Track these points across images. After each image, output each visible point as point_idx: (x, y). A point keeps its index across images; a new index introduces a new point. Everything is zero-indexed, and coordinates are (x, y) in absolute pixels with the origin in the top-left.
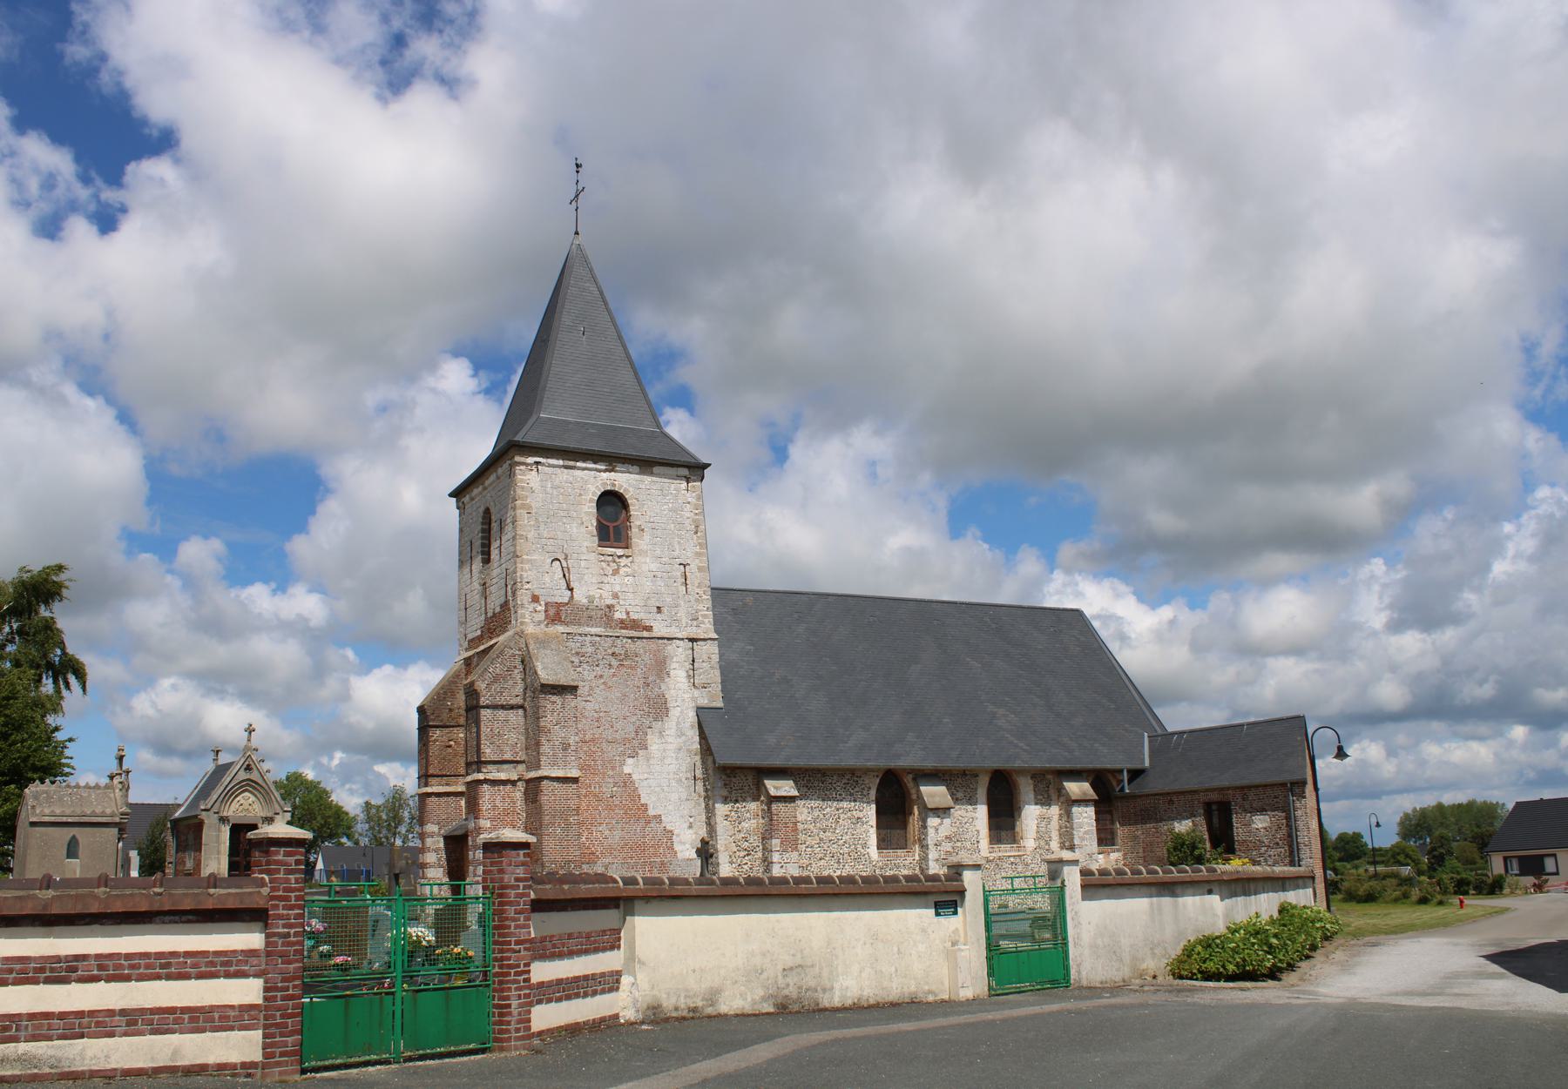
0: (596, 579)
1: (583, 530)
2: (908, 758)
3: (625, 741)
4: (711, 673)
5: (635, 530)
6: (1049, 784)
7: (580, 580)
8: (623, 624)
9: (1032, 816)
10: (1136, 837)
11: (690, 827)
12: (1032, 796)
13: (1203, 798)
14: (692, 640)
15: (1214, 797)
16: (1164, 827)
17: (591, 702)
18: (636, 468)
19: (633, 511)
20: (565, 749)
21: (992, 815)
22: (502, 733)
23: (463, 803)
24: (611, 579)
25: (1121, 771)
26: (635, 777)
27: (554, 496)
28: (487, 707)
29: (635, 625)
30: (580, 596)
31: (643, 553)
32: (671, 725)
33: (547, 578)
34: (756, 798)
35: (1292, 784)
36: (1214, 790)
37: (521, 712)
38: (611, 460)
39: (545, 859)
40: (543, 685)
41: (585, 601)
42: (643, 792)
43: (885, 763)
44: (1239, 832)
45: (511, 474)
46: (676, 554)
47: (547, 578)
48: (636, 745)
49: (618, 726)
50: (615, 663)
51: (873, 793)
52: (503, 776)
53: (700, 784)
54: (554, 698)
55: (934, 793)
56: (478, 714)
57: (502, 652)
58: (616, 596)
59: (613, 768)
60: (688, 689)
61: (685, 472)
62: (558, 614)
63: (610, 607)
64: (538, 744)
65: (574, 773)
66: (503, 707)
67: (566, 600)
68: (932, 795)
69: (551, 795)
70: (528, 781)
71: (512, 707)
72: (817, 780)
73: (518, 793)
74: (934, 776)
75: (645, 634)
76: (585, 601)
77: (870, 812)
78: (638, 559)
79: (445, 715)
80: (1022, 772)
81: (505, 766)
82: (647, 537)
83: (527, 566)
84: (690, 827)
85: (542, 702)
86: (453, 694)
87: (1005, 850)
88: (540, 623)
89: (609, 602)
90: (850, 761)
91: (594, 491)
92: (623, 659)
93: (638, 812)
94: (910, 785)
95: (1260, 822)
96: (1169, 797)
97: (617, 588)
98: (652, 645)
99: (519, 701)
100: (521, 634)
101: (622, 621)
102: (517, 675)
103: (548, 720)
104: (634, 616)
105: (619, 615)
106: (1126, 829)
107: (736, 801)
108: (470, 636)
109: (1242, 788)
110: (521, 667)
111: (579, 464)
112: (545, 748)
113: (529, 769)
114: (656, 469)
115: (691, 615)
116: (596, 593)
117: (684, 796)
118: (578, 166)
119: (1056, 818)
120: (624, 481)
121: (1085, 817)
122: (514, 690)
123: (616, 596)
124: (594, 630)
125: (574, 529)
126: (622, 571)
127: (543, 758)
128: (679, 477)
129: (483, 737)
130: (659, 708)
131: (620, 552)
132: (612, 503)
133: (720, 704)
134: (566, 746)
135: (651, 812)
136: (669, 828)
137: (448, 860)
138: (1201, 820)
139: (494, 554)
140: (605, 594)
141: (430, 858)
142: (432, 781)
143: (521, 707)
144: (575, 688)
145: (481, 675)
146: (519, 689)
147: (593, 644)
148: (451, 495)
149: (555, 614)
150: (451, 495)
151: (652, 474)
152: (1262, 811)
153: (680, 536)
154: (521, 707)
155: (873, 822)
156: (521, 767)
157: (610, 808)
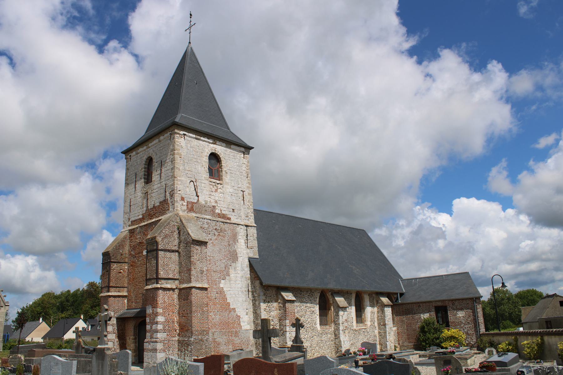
0: (208, 194)
1: (203, 169)
2: (332, 285)
3: (221, 271)
4: (254, 243)
5: (224, 172)
6: (375, 297)
7: (202, 192)
8: (219, 216)
9: (370, 312)
10: (403, 321)
11: (247, 314)
12: (369, 303)
13: (434, 304)
14: (247, 226)
15: (440, 304)
16: (416, 316)
17: (210, 250)
18: (224, 144)
19: (224, 163)
20: (202, 273)
21: (357, 311)
22: (169, 264)
23: (126, 301)
24: (214, 194)
25: (397, 294)
26: (225, 289)
27: (190, 151)
28: (162, 250)
29: (224, 216)
30: (202, 200)
31: (227, 183)
32: (239, 265)
33: (188, 190)
34: (276, 301)
35: (476, 298)
36: (439, 301)
37: (177, 254)
38: (215, 139)
39: (193, 329)
40: (193, 240)
41: (203, 203)
42: (228, 297)
43: (321, 287)
44: (451, 318)
45: (171, 138)
46: (240, 186)
47: (188, 190)
48: (225, 274)
49: (218, 264)
50: (217, 234)
51: (318, 300)
52: (169, 286)
53: (250, 294)
54: (197, 247)
55: (340, 300)
56: (157, 254)
57: (169, 223)
58: (216, 202)
59: (216, 285)
60: (246, 249)
61: (243, 149)
62: (192, 207)
63: (214, 207)
64: (189, 270)
65: (206, 286)
66: (169, 251)
67: (196, 201)
68: (340, 302)
69: (196, 296)
70: (180, 290)
71: (173, 251)
72: (301, 293)
73: (175, 295)
74: (340, 293)
75: (228, 221)
76: (203, 203)
77: (317, 308)
78: (225, 186)
79: (119, 257)
80: (365, 292)
81: (170, 281)
82: (228, 176)
83: (179, 183)
84: (247, 314)
85: (192, 249)
86: (123, 246)
87: (361, 326)
88: (184, 211)
89: (214, 204)
90: (312, 286)
91: (207, 152)
92: (220, 231)
93: (226, 307)
94: (330, 297)
95: (461, 314)
96: (419, 304)
97: (217, 198)
98: (231, 226)
99: (176, 248)
100: (177, 215)
101: (219, 214)
102: (176, 235)
103: (195, 258)
104: (223, 212)
105: (217, 211)
106: (398, 317)
107: (269, 302)
108: (133, 219)
109: (452, 300)
110: (177, 231)
111: (202, 138)
112: (193, 272)
113: (181, 283)
114: (232, 146)
115: (244, 215)
116: (208, 200)
117: (244, 299)
118: (191, 15)
119: (376, 312)
120: (220, 149)
121: (388, 311)
122: (174, 243)
123: (216, 202)
124: (208, 217)
125: (199, 168)
126: (219, 190)
127: (192, 277)
128: (240, 151)
129: (160, 266)
130: (234, 257)
131: (218, 182)
132: (214, 157)
133: (257, 257)
134: (202, 272)
135: (231, 307)
136: (238, 314)
137: (118, 330)
138: (433, 314)
139: (155, 177)
140: (212, 201)
141: (110, 328)
142: (111, 289)
143: (177, 251)
144: (206, 243)
145: (159, 234)
146: (176, 242)
147: (208, 223)
148: (122, 153)
149: (191, 207)
150: (122, 153)
151: (230, 148)
152: (462, 309)
153: (241, 178)
154: (177, 251)
155: (318, 313)
156: (177, 282)
157: (215, 304)
